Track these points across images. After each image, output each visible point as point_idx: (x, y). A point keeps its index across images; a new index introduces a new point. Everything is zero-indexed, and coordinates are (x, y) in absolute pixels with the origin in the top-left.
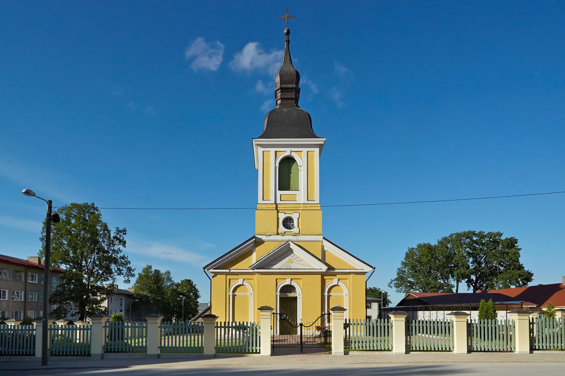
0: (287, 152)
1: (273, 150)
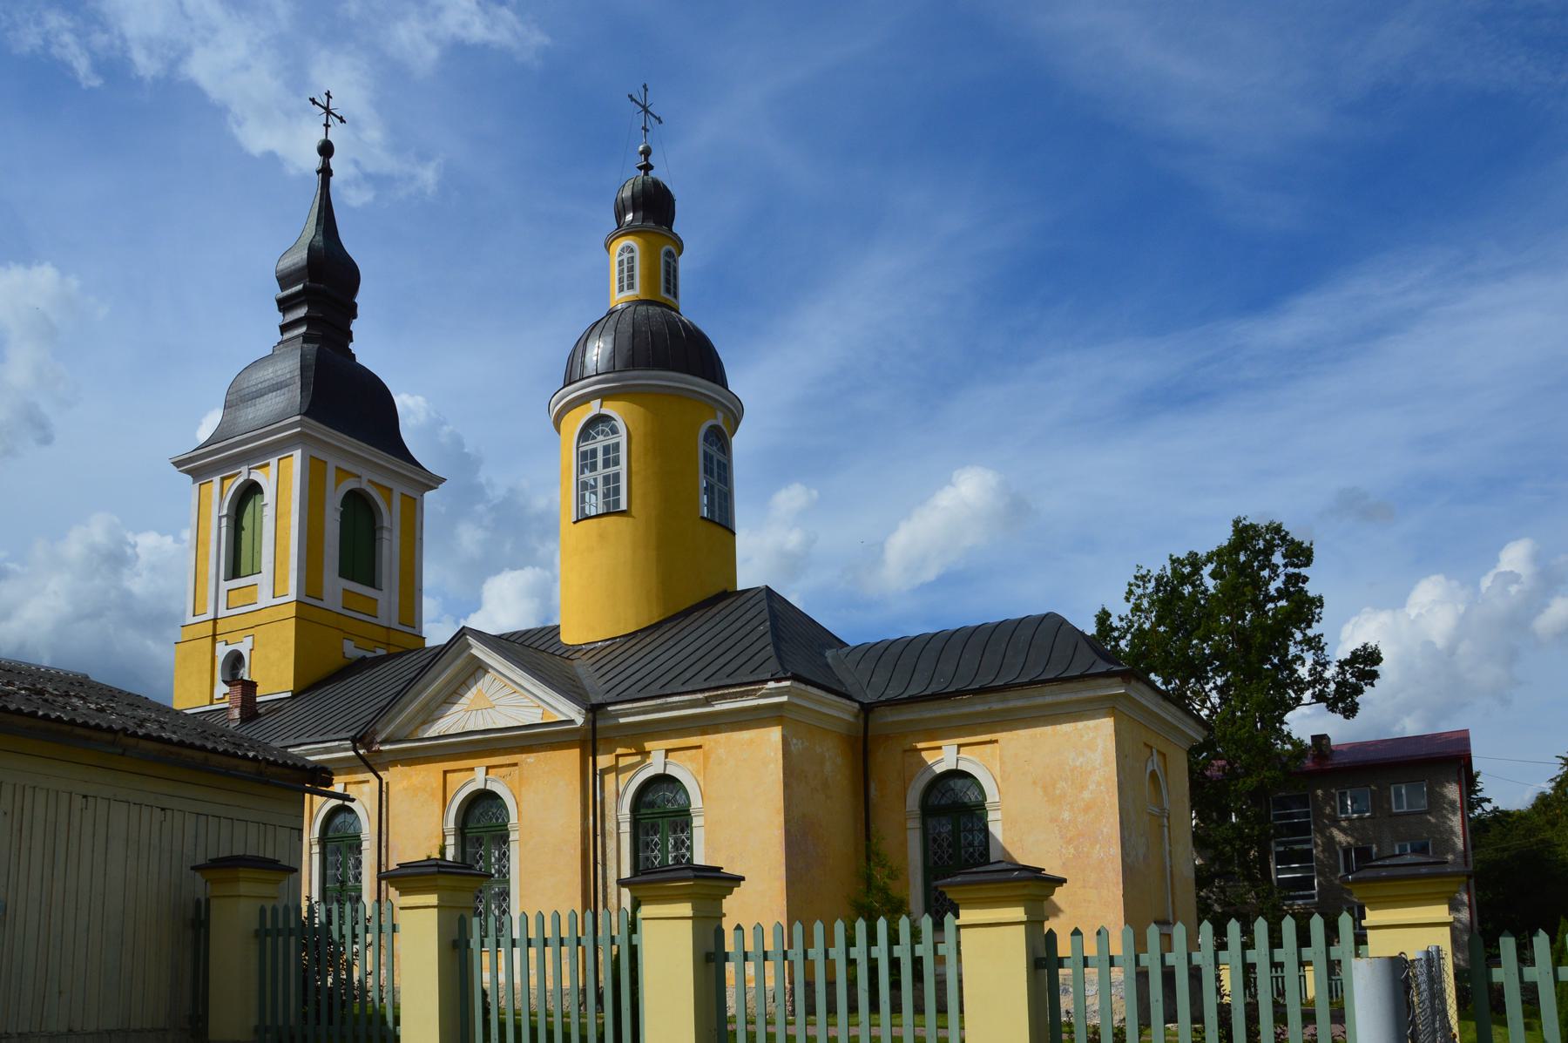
0: (365, 480)
1: (332, 462)
